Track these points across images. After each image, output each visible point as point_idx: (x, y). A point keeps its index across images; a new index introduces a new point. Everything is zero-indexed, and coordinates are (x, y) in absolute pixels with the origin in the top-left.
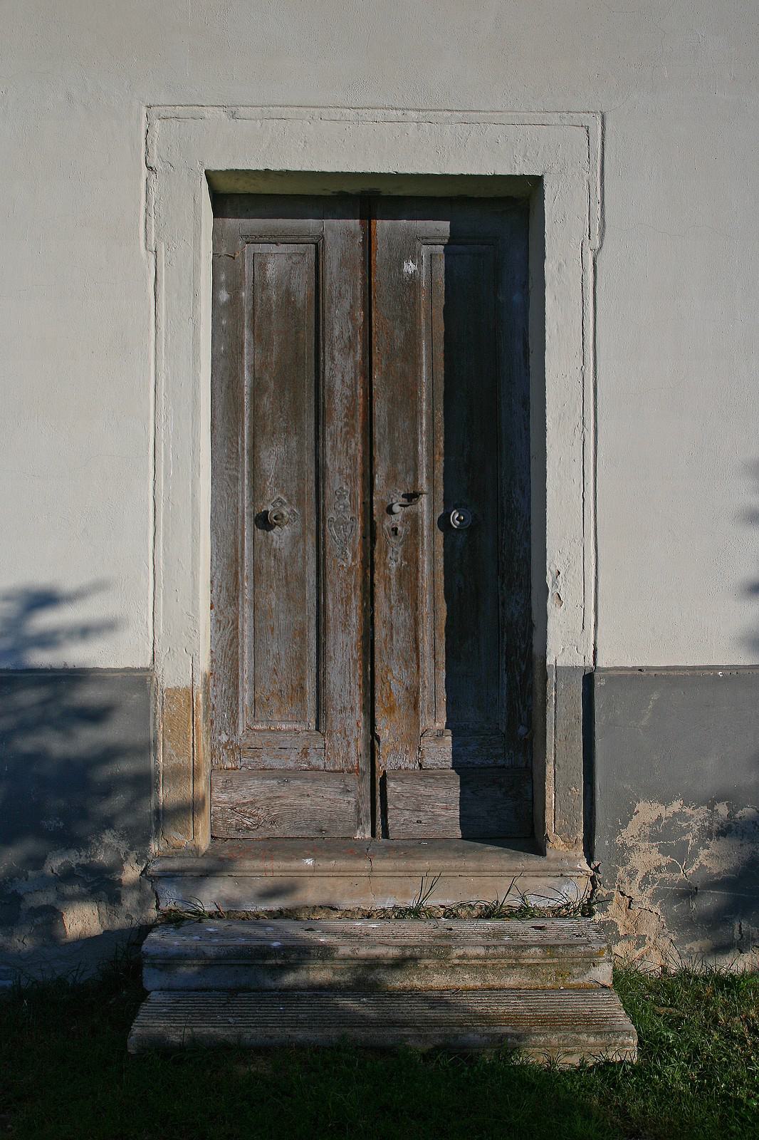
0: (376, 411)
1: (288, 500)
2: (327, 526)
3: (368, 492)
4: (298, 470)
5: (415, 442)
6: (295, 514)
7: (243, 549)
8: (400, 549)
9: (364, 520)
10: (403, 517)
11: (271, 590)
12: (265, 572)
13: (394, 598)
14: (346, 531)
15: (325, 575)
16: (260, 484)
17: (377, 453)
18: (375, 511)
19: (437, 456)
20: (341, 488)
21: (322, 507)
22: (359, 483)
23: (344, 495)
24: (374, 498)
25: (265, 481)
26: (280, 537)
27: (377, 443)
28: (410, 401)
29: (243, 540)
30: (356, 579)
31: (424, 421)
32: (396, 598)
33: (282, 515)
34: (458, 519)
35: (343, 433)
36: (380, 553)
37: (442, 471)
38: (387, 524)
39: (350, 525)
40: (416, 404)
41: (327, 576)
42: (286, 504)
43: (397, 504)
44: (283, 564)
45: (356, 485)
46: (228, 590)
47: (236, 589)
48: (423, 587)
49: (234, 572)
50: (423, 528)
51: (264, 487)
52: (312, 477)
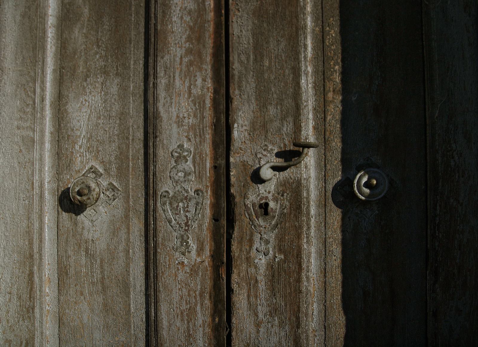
0: (235, 30)
1: (105, 170)
2: (159, 204)
3: (222, 150)
4: (120, 125)
5: (297, 73)
6: (114, 188)
7: (41, 241)
8: (272, 236)
9: (216, 194)
10: (277, 186)
11: (82, 298)
12: (73, 272)
13: (262, 310)
14: (188, 211)
15: (156, 277)
16: (67, 149)
17: (237, 92)
18: (233, 179)
19: (330, 95)
20: (181, 146)
21: (151, 177)
22: (208, 136)
23: (185, 157)
24: (232, 160)
25: (74, 143)
26: (97, 221)
27: (236, 77)
28: (287, 13)
29: (41, 229)
30: (203, 282)
31: (309, 42)
32: (266, 309)
33: (89, 187)
34: (367, 185)
35: (184, 64)
36: (240, 242)
37: (338, 117)
38: (254, 196)
39: (193, 202)
40: (297, 17)
41: (159, 278)
42: (102, 174)
43: (268, 165)
44: (98, 261)
45: (202, 140)
46: (20, 298)
47: (31, 297)
48: (308, 291)
49: (28, 272)
50: (309, 202)
51: (72, 153)
52: (140, 135)
